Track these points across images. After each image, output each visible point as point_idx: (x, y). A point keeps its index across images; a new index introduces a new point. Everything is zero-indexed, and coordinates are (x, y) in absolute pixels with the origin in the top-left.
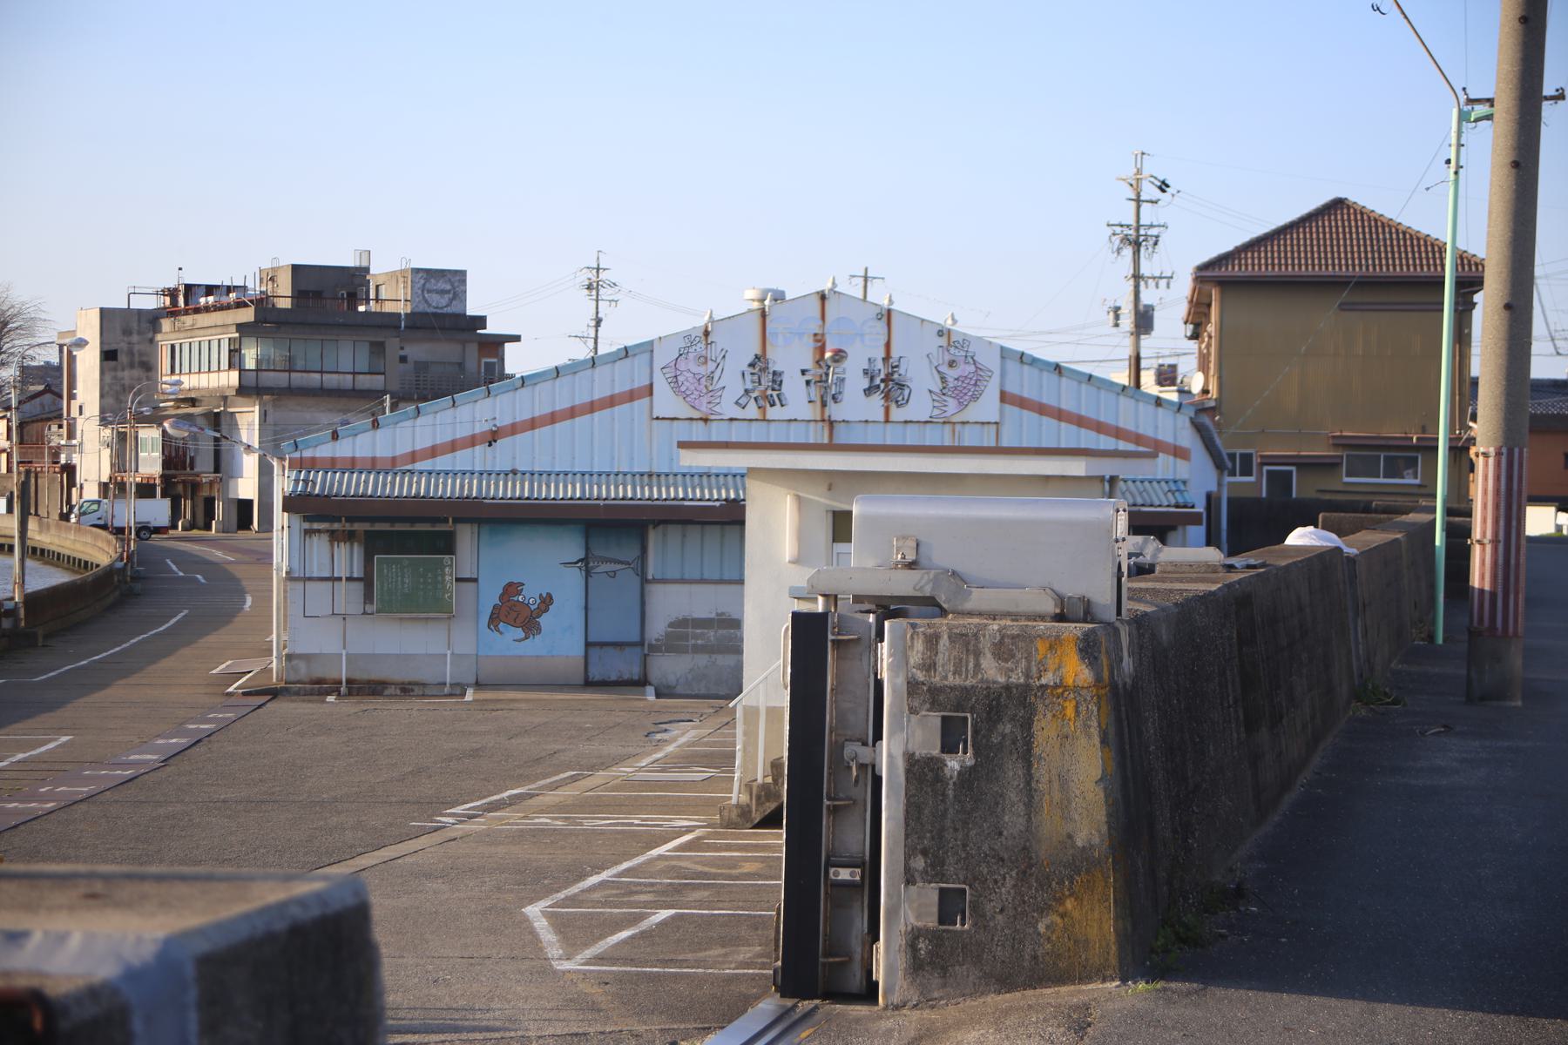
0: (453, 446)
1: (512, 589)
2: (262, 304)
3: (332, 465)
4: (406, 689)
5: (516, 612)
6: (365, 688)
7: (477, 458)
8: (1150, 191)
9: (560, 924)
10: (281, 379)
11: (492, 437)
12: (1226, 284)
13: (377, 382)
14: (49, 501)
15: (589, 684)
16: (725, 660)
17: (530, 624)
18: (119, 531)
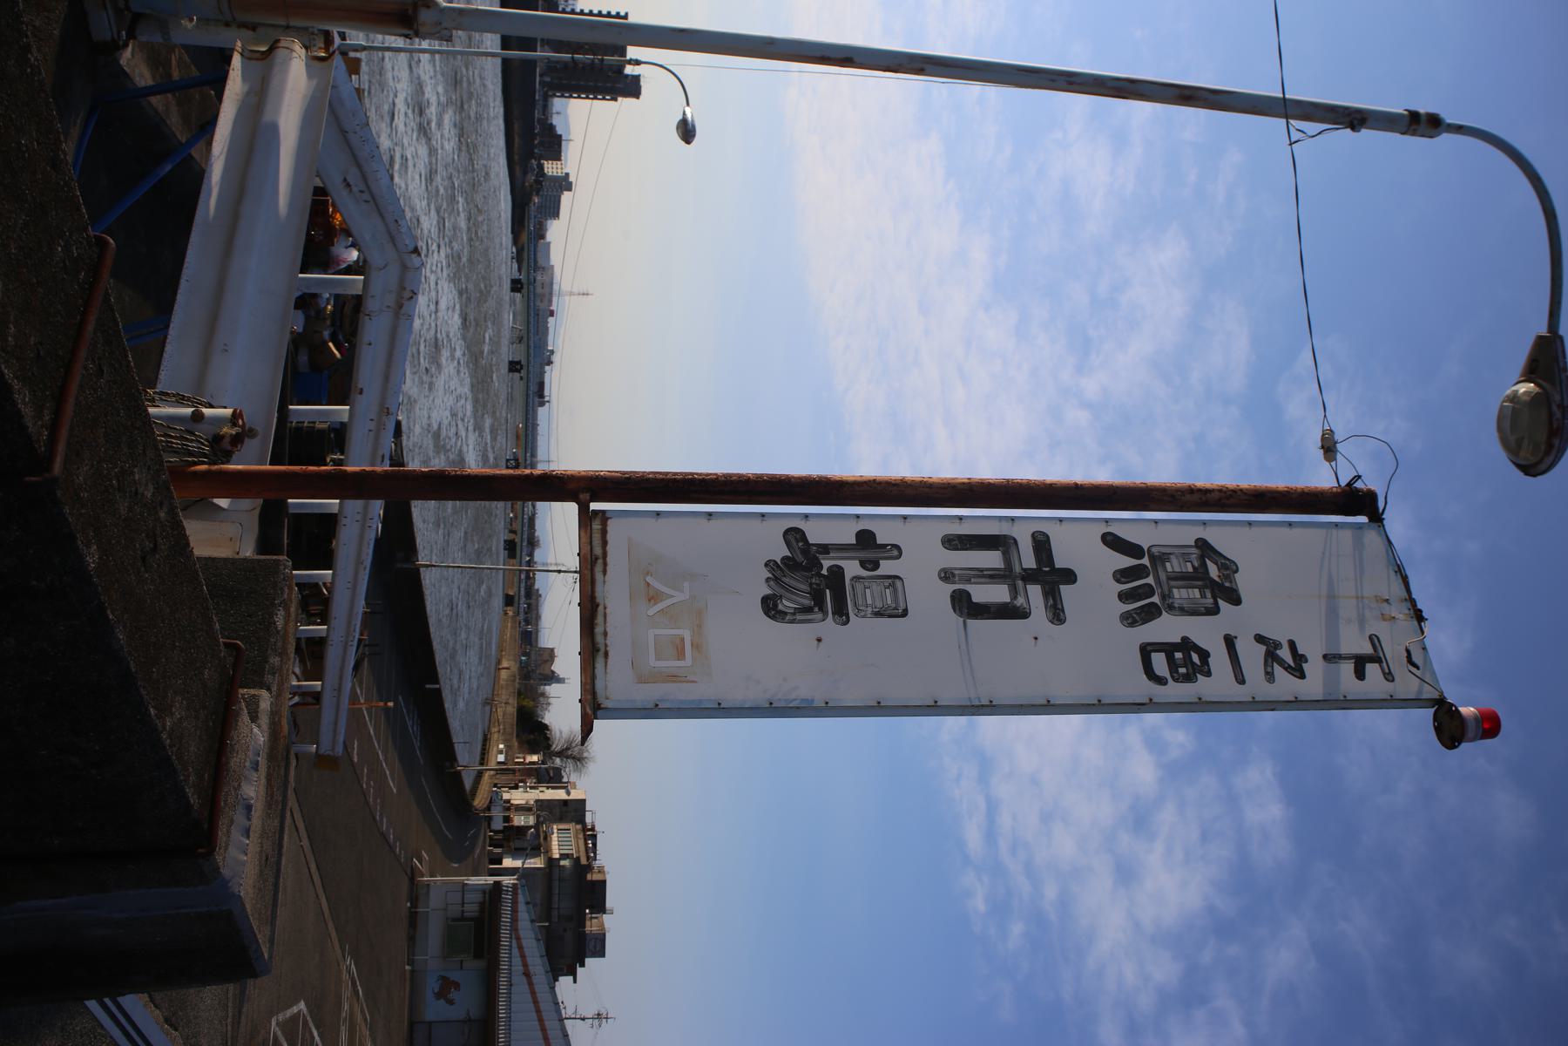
0: (523, 957)
1: (457, 986)
2: (589, 868)
3: (515, 902)
4: (412, 939)
5: (446, 988)
6: (413, 919)
7: (518, 967)
9: (295, 1018)
10: (556, 876)
11: (527, 974)
13: (555, 919)
14: (503, 778)
15: (412, 1025)
17: (442, 994)
18: (488, 809)
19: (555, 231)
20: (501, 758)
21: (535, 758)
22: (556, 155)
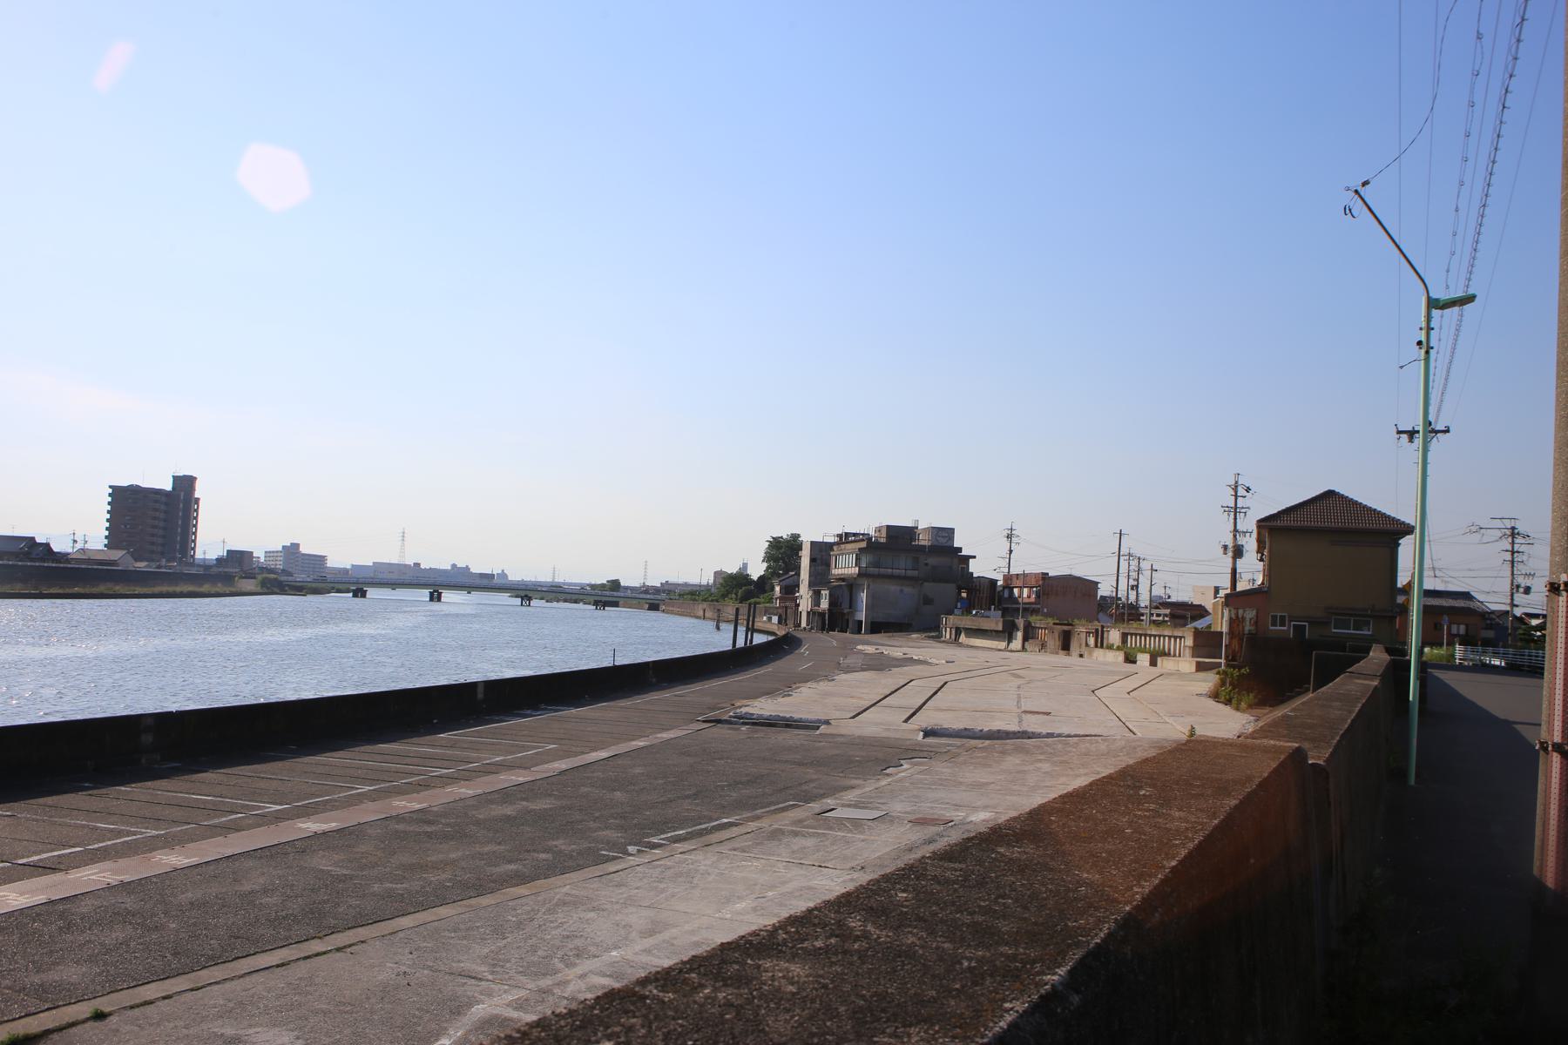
8: (1241, 492)
10: (875, 571)
12: (1272, 530)
16: (480, 690)
19: (340, 558)
20: (775, 619)
21: (777, 589)
22: (993, 582)
